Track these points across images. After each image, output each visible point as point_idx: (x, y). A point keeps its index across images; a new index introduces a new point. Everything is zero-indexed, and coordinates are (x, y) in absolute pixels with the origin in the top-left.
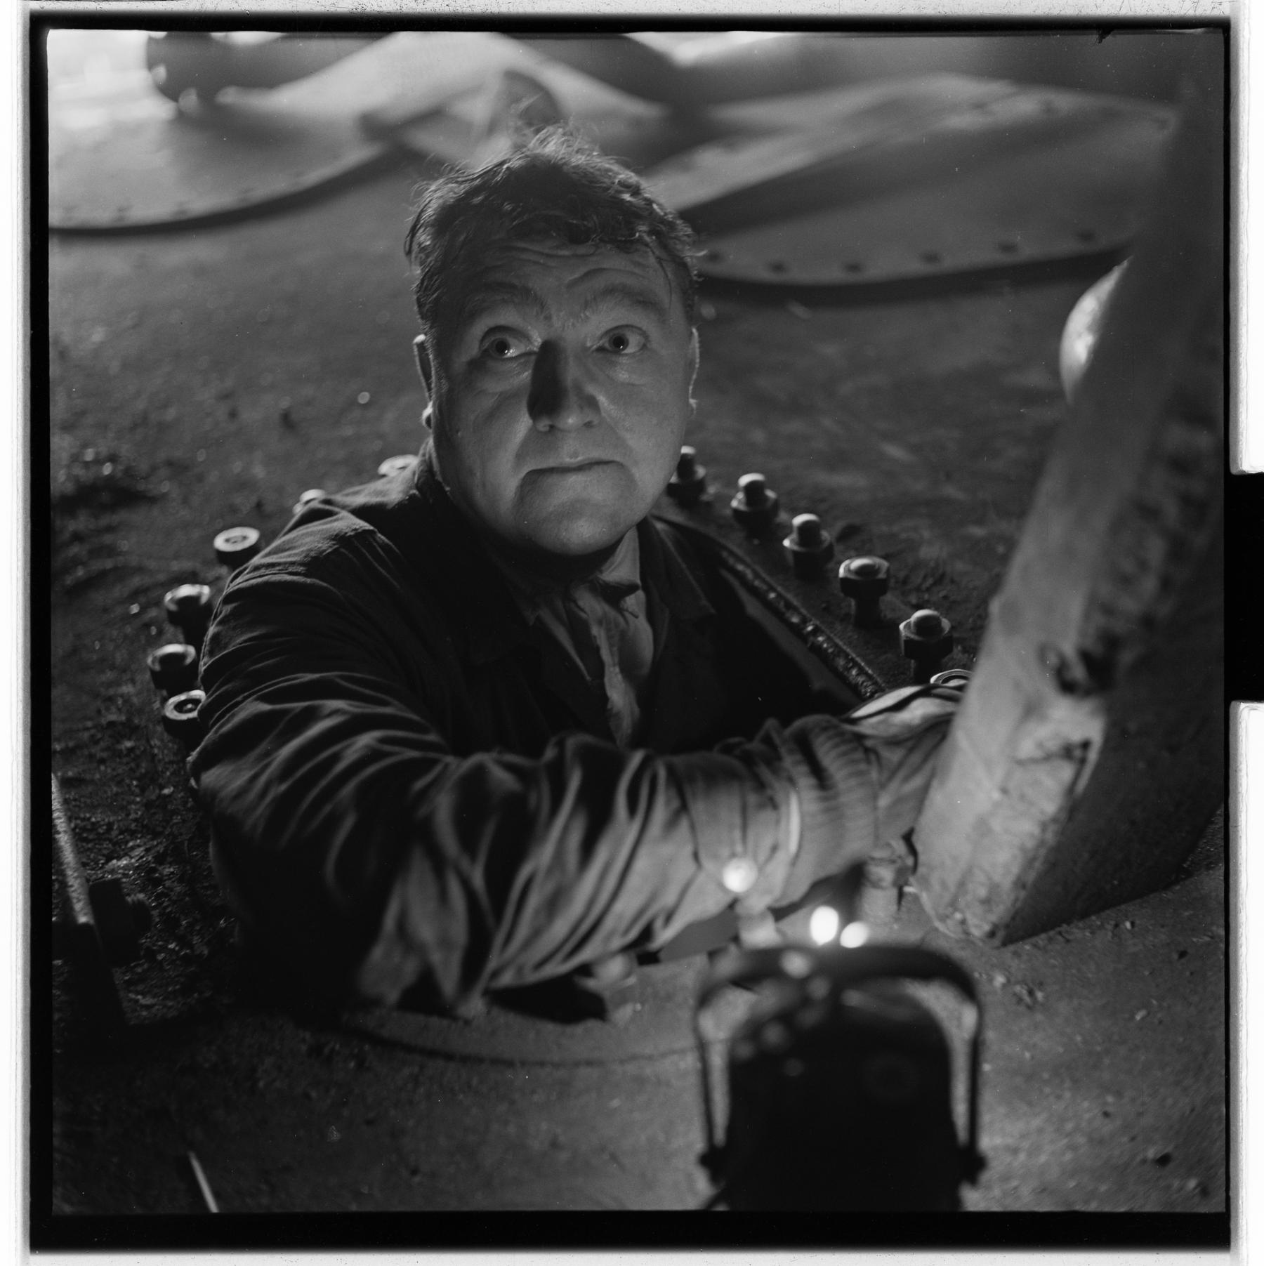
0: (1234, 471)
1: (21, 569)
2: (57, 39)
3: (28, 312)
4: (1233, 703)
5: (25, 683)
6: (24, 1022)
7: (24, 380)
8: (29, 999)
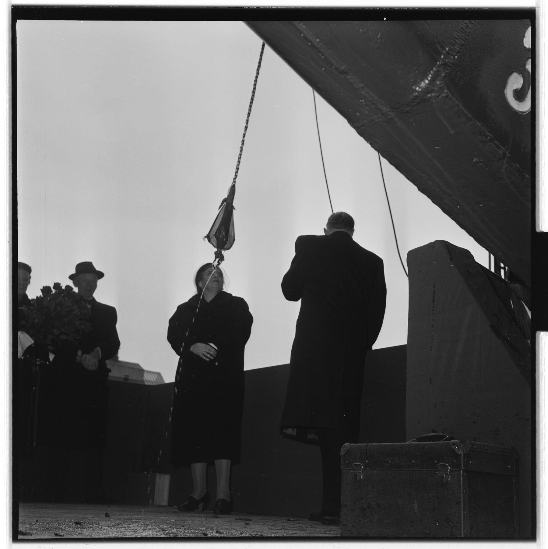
1: (8, 274)
2: (20, 23)
4: (538, 332)
8: (11, 462)
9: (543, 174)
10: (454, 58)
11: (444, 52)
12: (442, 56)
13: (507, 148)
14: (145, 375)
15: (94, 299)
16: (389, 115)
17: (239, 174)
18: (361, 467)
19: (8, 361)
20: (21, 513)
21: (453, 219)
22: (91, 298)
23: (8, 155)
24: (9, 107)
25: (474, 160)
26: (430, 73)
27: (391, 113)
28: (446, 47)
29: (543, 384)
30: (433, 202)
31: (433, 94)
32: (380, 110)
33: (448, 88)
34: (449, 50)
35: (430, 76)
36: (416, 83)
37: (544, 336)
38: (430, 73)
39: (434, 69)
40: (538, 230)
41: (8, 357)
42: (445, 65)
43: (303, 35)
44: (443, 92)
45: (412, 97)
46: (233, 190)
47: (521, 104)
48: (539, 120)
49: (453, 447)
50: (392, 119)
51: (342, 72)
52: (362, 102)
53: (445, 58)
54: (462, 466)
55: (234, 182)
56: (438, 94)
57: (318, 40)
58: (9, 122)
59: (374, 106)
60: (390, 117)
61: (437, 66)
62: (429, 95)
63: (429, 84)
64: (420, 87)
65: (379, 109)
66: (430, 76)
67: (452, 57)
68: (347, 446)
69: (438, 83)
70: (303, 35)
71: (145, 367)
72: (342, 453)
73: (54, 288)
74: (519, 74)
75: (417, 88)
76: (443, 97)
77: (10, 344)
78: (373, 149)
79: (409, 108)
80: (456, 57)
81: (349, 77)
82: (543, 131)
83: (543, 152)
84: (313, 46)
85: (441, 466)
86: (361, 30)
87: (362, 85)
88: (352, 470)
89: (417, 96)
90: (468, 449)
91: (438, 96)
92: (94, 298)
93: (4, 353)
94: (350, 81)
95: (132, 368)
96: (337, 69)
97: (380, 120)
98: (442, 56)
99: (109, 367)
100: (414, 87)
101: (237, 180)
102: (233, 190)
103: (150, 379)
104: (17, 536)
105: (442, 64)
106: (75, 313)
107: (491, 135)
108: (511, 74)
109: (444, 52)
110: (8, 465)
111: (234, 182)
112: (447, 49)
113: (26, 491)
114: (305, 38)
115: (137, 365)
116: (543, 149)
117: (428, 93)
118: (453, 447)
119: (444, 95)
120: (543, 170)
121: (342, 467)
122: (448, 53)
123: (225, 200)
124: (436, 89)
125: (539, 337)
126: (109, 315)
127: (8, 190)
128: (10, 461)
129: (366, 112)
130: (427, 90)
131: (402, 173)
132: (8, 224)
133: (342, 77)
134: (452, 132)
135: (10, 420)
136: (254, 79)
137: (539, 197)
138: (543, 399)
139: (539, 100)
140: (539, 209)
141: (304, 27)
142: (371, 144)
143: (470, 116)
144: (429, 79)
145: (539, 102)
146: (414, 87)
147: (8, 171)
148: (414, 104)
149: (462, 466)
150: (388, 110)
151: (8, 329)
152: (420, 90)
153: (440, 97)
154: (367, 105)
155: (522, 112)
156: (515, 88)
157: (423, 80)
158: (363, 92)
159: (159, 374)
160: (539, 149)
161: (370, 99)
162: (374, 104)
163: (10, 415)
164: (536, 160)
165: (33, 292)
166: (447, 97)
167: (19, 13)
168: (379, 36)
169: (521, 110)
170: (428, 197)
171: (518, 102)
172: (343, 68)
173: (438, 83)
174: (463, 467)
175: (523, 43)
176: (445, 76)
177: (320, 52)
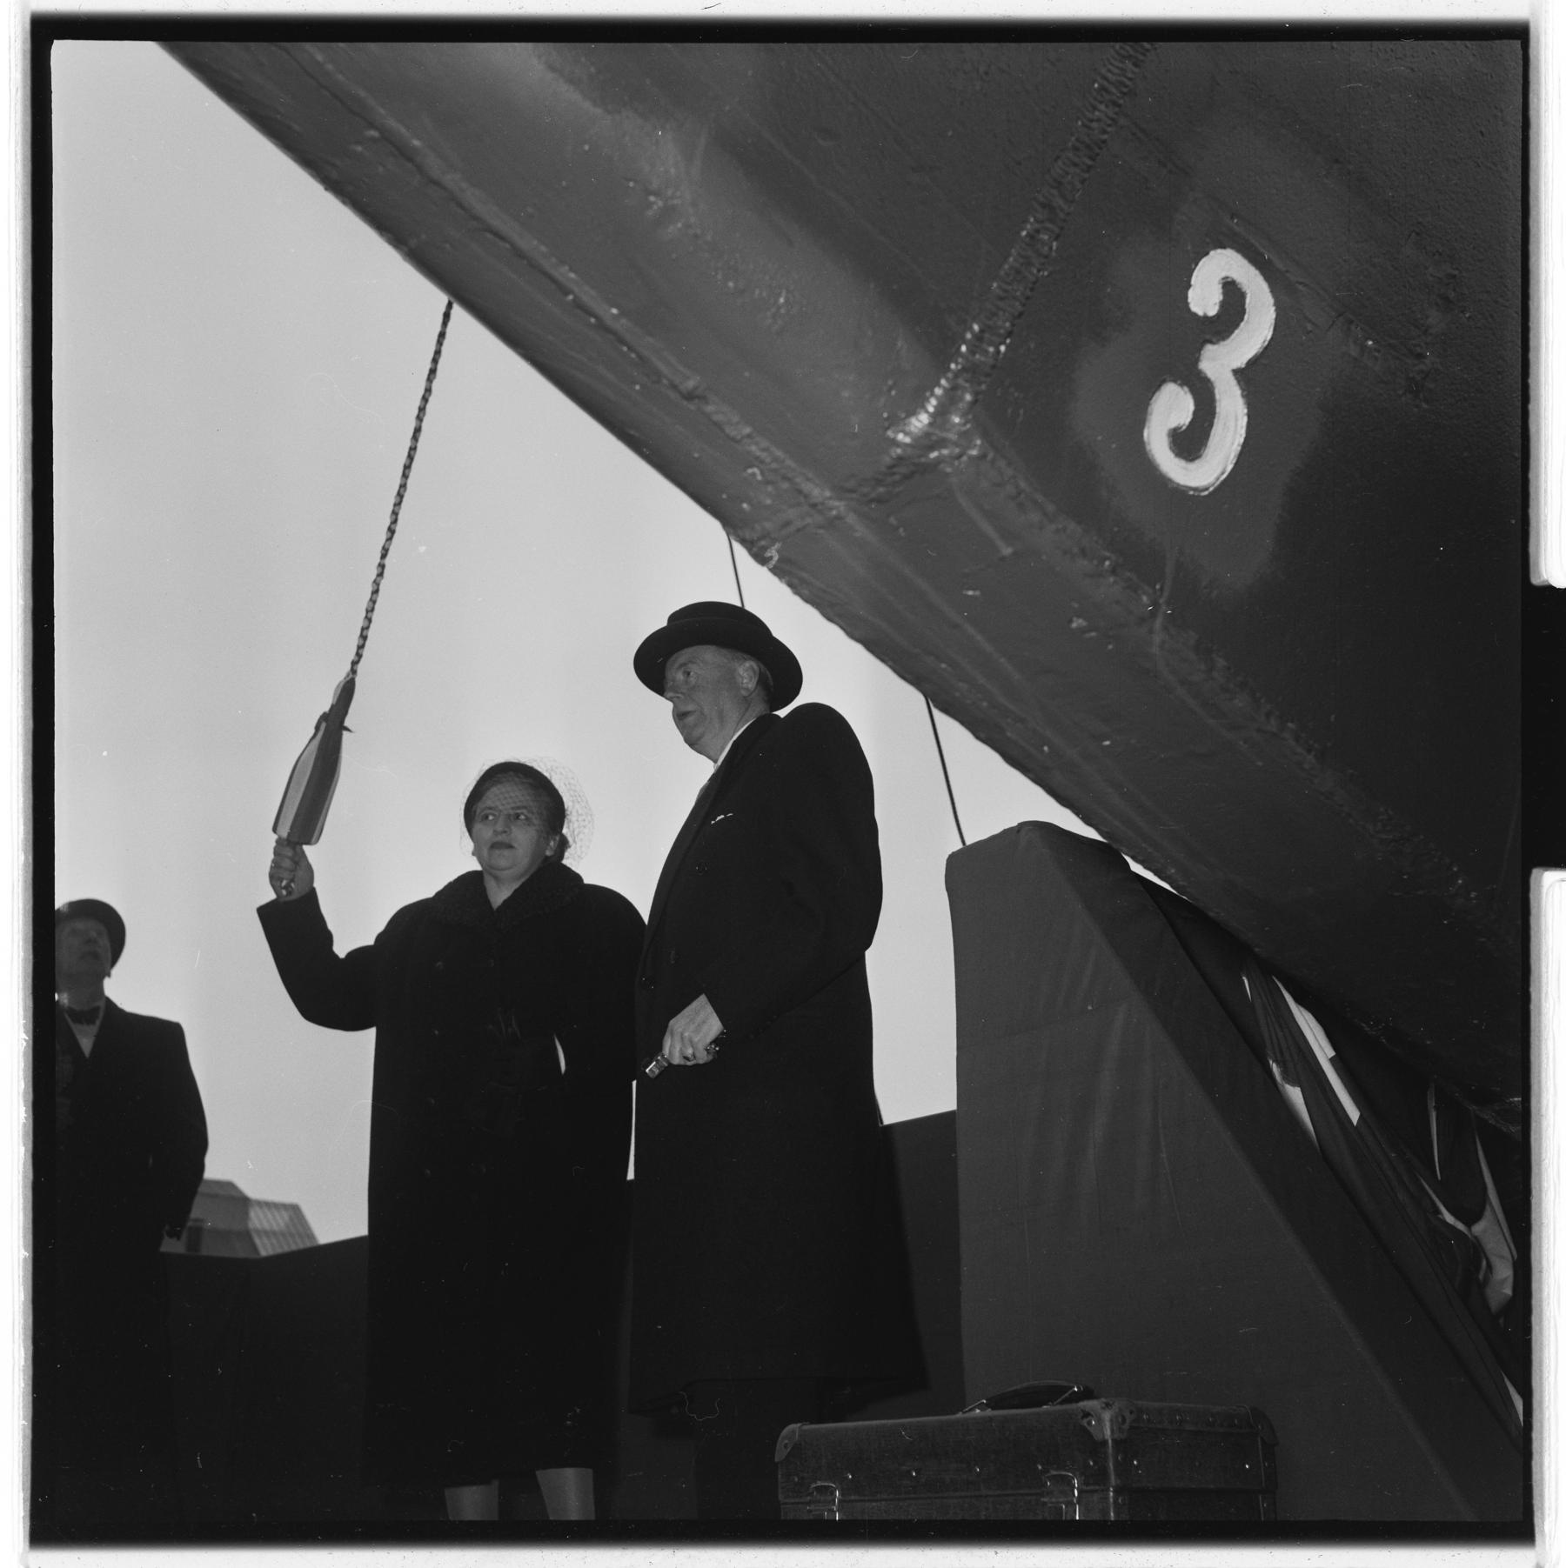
0: (1535, 581)
2: (61, 50)
3: (29, 575)
4: (1535, 872)
6: (25, 889)
10: (998, 352)
11: (969, 336)
12: (964, 348)
13: (1162, 589)
14: (252, 1214)
15: (110, 1004)
16: (831, 509)
17: (366, 652)
18: (833, 1493)
21: (1038, 781)
25: (1074, 625)
26: (933, 394)
27: (837, 503)
28: (974, 320)
30: (978, 737)
31: (945, 452)
32: (806, 496)
33: (985, 435)
34: (982, 331)
35: (934, 402)
36: (896, 421)
38: (933, 394)
39: (943, 382)
42: (971, 370)
43: (571, 297)
44: (970, 446)
45: (887, 460)
46: (346, 693)
47: (1192, 466)
49: (1084, 1422)
50: (838, 518)
51: (690, 396)
52: (754, 475)
53: (972, 351)
54: (1113, 1477)
55: (353, 671)
56: (957, 450)
57: (615, 311)
59: (785, 485)
60: (834, 512)
61: (950, 375)
62: (934, 455)
63: (930, 424)
64: (906, 434)
65: (800, 492)
66: (934, 402)
67: (991, 349)
68: (794, 1431)
69: (957, 420)
70: (571, 297)
71: (251, 1190)
72: (780, 1454)
74: (1181, 385)
75: (901, 437)
76: (971, 458)
78: (797, 599)
79: (881, 490)
80: (1003, 348)
81: (710, 408)
84: (602, 326)
85: (1053, 1478)
86: (731, 284)
87: (748, 430)
88: (809, 1503)
89: (900, 458)
90: (1126, 1426)
91: (959, 457)
94: (716, 418)
95: (216, 1196)
96: (674, 387)
97: (809, 520)
98: (964, 348)
100: (890, 433)
101: (360, 668)
102: (346, 693)
103: (266, 1226)
105: (964, 369)
107: (1114, 557)
108: (1159, 387)
109: (969, 336)
111: (353, 671)
112: (976, 327)
114: (578, 305)
115: (230, 1185)
117: (932, 448)
118: (1084, 1422)
119: (974, 452)
121: (781, 1497)
122: (979, 338)
124: (952, 436)
126: (165, 1039)
129: (769, 502)
130: (927, 441)
131: (883, 660)
133: (692, 407)
134: (1007, 551)
136: (417, 403)
141: (572, 275)
142: (790, 585)
143: (1051, 508)
144: (931, 409)
146: (890, 433)
148: (897, 477)
149: (1113, 1477)
150: (828, 494)
152: (908, 440)
153: (965, 458)
154: (768, 482)
155: (1195, 489)
156: (1173, 425)
157: (912, 413)
158: (753, 448)
159: (294, 1210)
161: (774, 466)
162: (785, 478)
166: (983, 457)
168: (782, 300)
169: (1193, 484)
170: (962, 723)
171: (1182, 463)
172: (691, 384)
173: (957, 420)
174: (1113, 1479)
175: (1187, 304)
176: (975, 402)
177: (622, 341)
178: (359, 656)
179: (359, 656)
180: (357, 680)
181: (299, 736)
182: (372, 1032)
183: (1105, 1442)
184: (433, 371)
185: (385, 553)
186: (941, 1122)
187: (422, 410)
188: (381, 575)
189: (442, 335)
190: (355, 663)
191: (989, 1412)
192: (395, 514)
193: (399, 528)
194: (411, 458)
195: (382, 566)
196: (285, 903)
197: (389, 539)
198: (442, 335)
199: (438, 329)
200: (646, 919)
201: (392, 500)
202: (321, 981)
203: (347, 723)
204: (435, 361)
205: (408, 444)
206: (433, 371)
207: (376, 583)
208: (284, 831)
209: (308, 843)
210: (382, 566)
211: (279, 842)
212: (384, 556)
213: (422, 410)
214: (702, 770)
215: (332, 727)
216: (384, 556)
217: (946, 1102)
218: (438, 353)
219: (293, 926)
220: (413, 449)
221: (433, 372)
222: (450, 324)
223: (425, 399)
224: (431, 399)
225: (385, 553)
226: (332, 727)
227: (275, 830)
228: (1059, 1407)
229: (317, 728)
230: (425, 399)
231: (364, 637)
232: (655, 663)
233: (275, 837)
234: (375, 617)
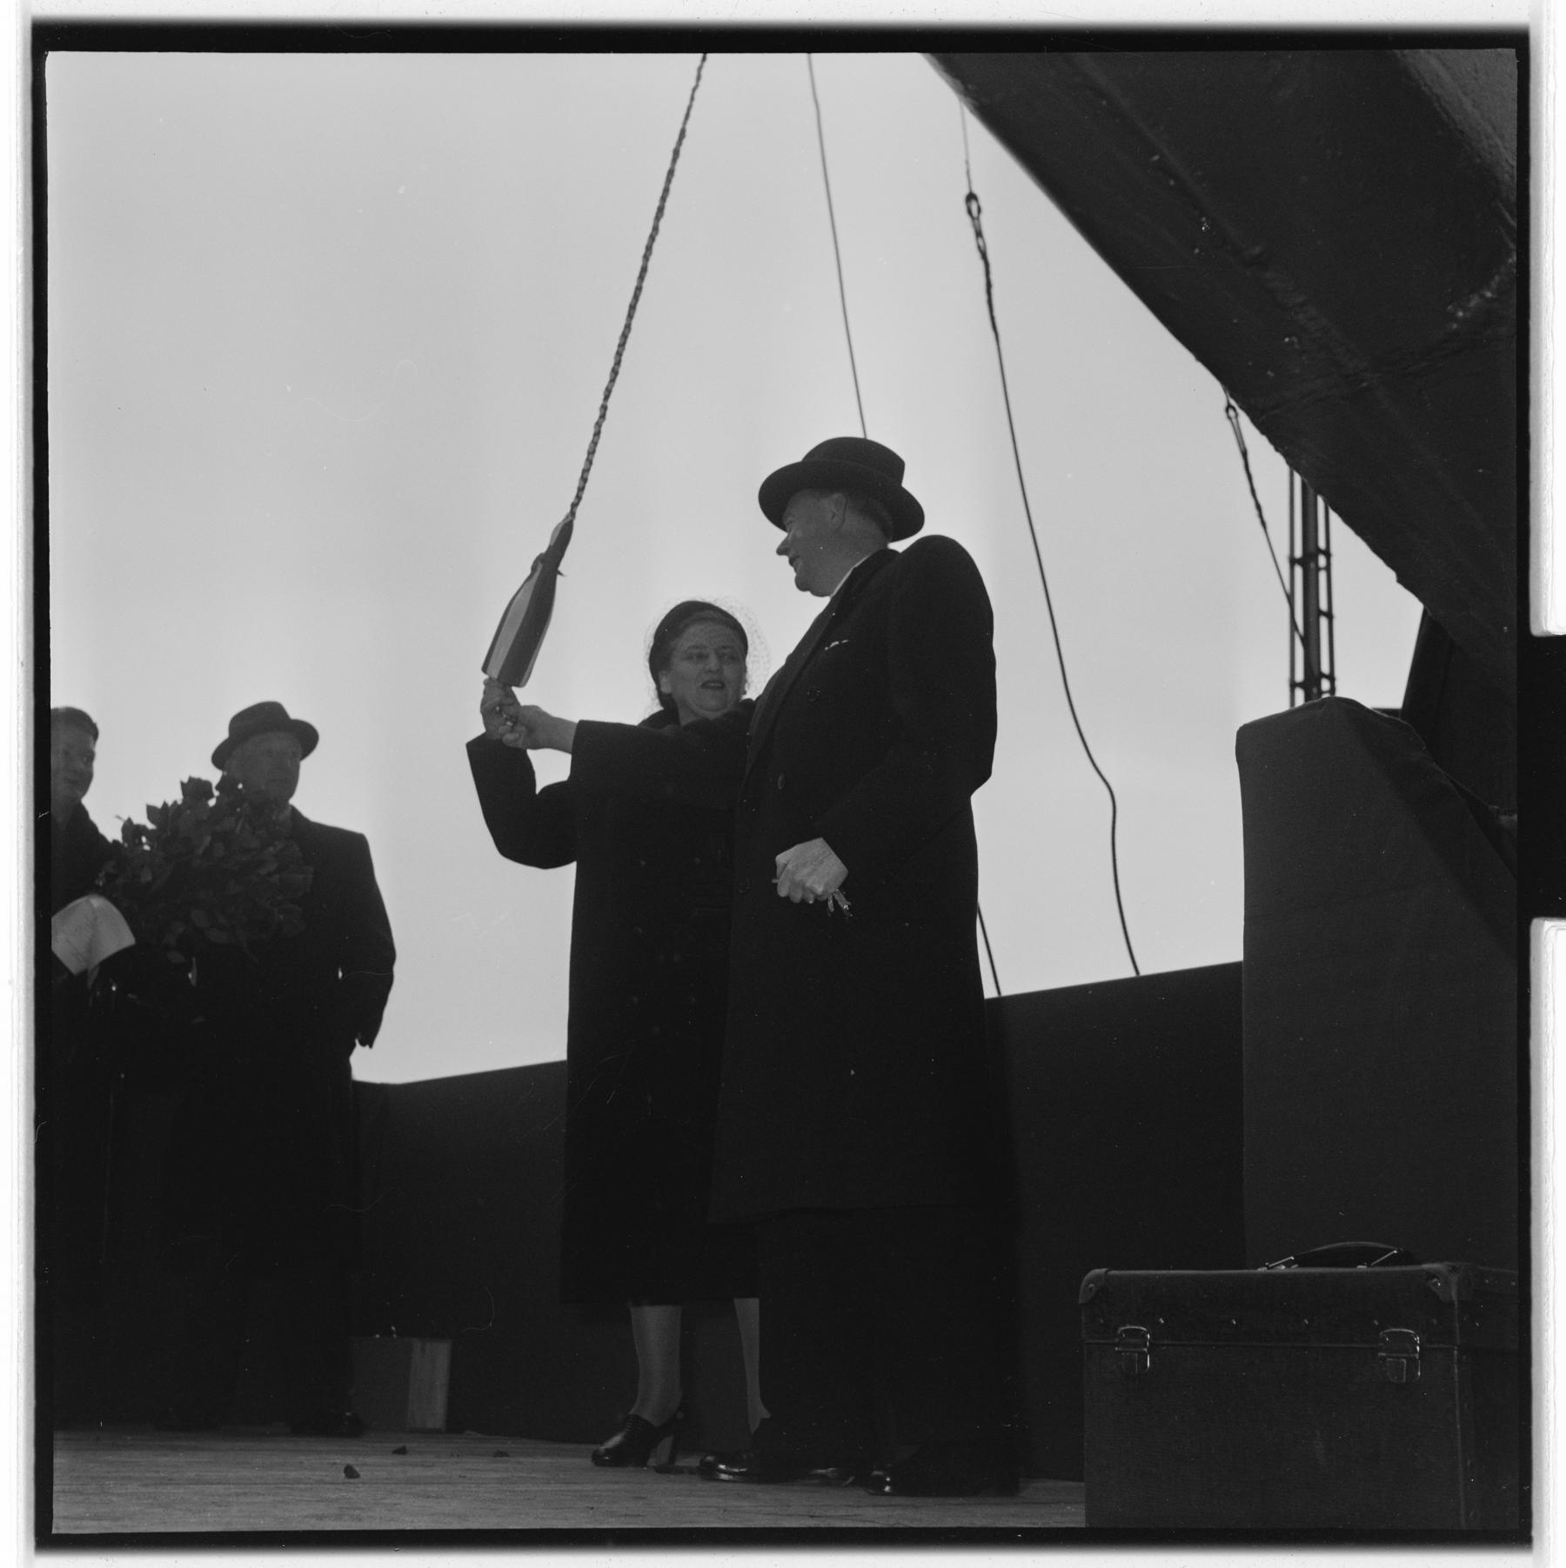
1: (22, 757)
2: (56, 61)
4: (1536, 922)
5: (27, 1071)
7: (26, 521)
8: (32, 1294)
9: (1549, 469)
17: (585, 495)
19: (22, 1005)
20: (60, 1461)
22: (288, 812)
23: (20, 38)
24: (25, 278)
29: (1550, 1070)
37: (1552, 933)
40: (1536, 631)
41: (22, 995)
43: (1156, 158)
46: (564, 535)
48: (1539, 316)
55: (573, 513)
58: (26, 322)
70: (1156, 158)
73: (218, 787)
77: (27, 956)
82: (1550, 346)
83: (1549, 405)
92: (294, 811)
93: (10, 983)
99: (757, 1425)
101: (579, 511)
102: (564, 535)
104: (46, 1537)
106: (263, 871)
110: (22, 1303)
111: (573, 513)
113: (74, 1400)
116: (1549, 397)
120: (1549, 457)
123: (541, 559)
125: (1539, 934)
127: (21, 516)
128: (27, 1290)
132: (21, 613)
135: (28, 1172)
136: (645, 241)
137: (1538, 536)
138: (1550, 1110)
139: (1539, 257)
140: (1539, 569)
145: (1538, 264)
147: (21, 461)
151: (22, 912)
160: (1539, 398)
163: (27, 1157)
164: (1532, 430)
165: (117, 802)
167: (50, 37)
178: (579, 498)
179: (579, 498)
180: (576, 523)
181: (515, 575)
182: (571, 869)
183: (1451, 1304)
184: (660, 211)
185: (608, 393)
186: (1237, 965)
187: (649, 249)
188: (603, 417)
189: (671, 173)
190: (574, 505)
191: (1295, 1268)
192: (619, 354)
193: (621, 370)
194: (636, 297)
195: (604, 408)
196: (703, 727)
197: (613, 380)
198: (671, 173)
199: (667, 166)
200: (538, 790)
201: (617, 341)
202: (522, 823)
203: (561, 568)
204: (663, 199)
205: (634, 284)
206: (660, 211)
207: (598, 425)
208: (495, 671)
209: (518, 685)
210: (604, 408)
211: (487, 683)
212: (606, 398)
213: (649, 249)
214: (818, 605)
215: (547, 568)
216: (606, 398)
217: (1222, 943)
218: (666, 191)
219: (497, 765)
220: (639, 289)
221: (661, 210)
222: (679, 162)
223: (652, 238)
224: (658, 238)
225: (608, 393)
226: (547, 568)
227: (485, 669)
228: (1378, 1269)
229: (534, 569)
230: (652, 238)
231: (584, 479)
232: (780, 496)
233: (486, 677)
234: (596, 460)
